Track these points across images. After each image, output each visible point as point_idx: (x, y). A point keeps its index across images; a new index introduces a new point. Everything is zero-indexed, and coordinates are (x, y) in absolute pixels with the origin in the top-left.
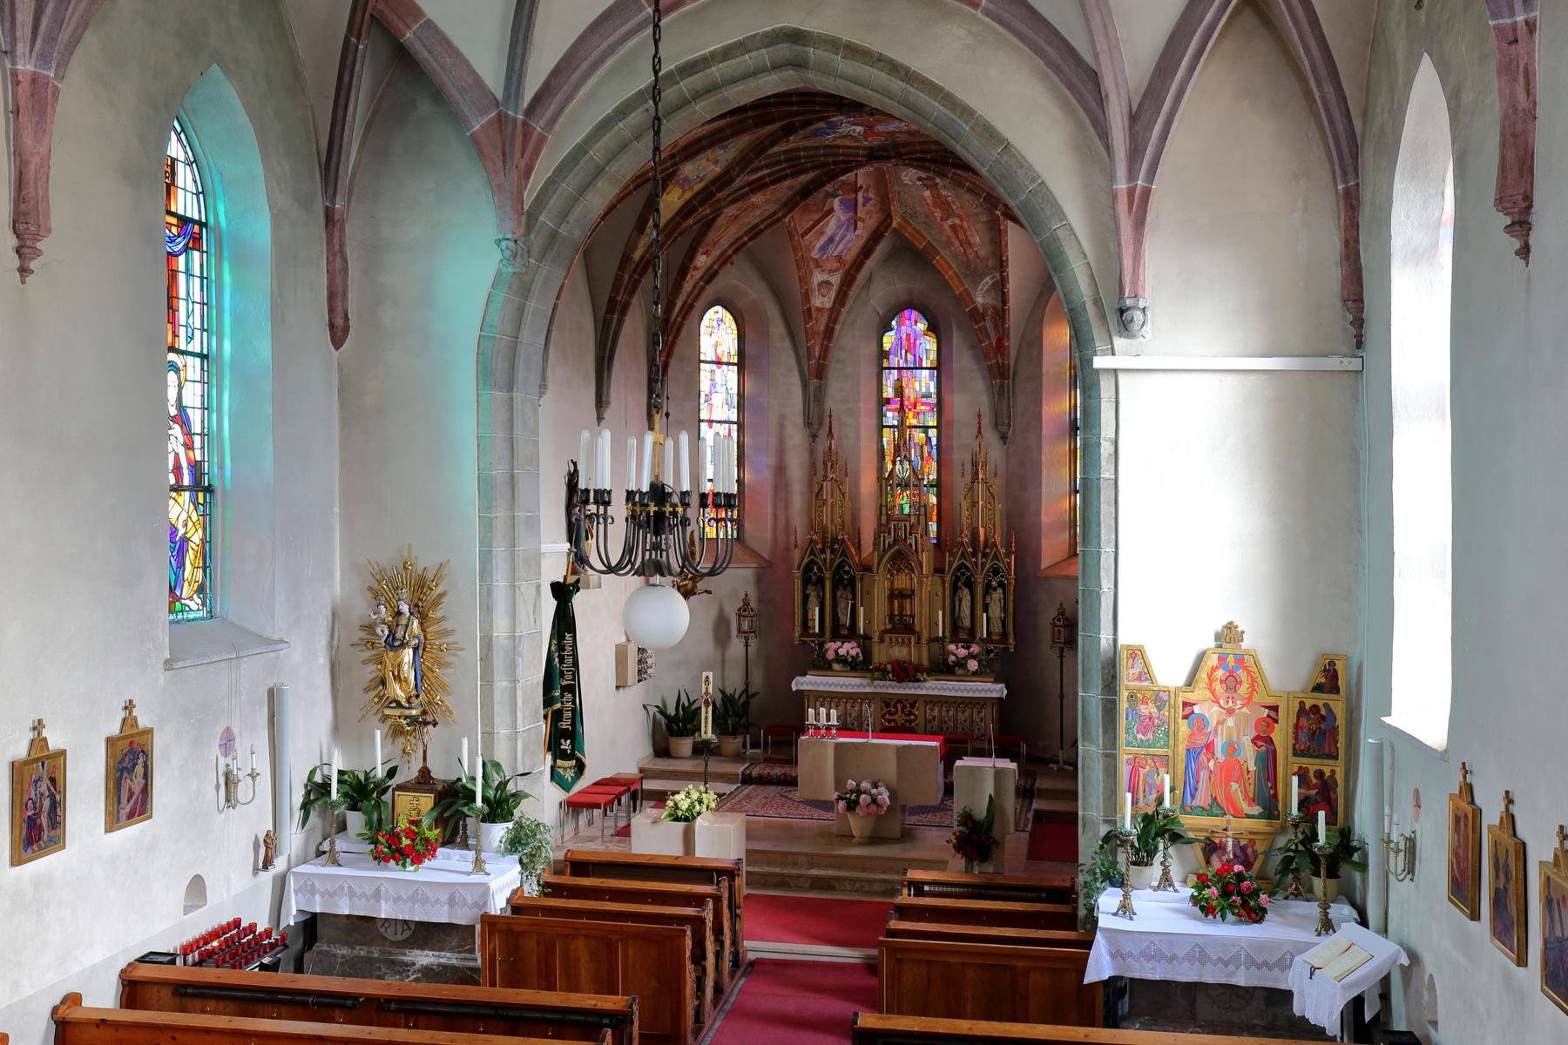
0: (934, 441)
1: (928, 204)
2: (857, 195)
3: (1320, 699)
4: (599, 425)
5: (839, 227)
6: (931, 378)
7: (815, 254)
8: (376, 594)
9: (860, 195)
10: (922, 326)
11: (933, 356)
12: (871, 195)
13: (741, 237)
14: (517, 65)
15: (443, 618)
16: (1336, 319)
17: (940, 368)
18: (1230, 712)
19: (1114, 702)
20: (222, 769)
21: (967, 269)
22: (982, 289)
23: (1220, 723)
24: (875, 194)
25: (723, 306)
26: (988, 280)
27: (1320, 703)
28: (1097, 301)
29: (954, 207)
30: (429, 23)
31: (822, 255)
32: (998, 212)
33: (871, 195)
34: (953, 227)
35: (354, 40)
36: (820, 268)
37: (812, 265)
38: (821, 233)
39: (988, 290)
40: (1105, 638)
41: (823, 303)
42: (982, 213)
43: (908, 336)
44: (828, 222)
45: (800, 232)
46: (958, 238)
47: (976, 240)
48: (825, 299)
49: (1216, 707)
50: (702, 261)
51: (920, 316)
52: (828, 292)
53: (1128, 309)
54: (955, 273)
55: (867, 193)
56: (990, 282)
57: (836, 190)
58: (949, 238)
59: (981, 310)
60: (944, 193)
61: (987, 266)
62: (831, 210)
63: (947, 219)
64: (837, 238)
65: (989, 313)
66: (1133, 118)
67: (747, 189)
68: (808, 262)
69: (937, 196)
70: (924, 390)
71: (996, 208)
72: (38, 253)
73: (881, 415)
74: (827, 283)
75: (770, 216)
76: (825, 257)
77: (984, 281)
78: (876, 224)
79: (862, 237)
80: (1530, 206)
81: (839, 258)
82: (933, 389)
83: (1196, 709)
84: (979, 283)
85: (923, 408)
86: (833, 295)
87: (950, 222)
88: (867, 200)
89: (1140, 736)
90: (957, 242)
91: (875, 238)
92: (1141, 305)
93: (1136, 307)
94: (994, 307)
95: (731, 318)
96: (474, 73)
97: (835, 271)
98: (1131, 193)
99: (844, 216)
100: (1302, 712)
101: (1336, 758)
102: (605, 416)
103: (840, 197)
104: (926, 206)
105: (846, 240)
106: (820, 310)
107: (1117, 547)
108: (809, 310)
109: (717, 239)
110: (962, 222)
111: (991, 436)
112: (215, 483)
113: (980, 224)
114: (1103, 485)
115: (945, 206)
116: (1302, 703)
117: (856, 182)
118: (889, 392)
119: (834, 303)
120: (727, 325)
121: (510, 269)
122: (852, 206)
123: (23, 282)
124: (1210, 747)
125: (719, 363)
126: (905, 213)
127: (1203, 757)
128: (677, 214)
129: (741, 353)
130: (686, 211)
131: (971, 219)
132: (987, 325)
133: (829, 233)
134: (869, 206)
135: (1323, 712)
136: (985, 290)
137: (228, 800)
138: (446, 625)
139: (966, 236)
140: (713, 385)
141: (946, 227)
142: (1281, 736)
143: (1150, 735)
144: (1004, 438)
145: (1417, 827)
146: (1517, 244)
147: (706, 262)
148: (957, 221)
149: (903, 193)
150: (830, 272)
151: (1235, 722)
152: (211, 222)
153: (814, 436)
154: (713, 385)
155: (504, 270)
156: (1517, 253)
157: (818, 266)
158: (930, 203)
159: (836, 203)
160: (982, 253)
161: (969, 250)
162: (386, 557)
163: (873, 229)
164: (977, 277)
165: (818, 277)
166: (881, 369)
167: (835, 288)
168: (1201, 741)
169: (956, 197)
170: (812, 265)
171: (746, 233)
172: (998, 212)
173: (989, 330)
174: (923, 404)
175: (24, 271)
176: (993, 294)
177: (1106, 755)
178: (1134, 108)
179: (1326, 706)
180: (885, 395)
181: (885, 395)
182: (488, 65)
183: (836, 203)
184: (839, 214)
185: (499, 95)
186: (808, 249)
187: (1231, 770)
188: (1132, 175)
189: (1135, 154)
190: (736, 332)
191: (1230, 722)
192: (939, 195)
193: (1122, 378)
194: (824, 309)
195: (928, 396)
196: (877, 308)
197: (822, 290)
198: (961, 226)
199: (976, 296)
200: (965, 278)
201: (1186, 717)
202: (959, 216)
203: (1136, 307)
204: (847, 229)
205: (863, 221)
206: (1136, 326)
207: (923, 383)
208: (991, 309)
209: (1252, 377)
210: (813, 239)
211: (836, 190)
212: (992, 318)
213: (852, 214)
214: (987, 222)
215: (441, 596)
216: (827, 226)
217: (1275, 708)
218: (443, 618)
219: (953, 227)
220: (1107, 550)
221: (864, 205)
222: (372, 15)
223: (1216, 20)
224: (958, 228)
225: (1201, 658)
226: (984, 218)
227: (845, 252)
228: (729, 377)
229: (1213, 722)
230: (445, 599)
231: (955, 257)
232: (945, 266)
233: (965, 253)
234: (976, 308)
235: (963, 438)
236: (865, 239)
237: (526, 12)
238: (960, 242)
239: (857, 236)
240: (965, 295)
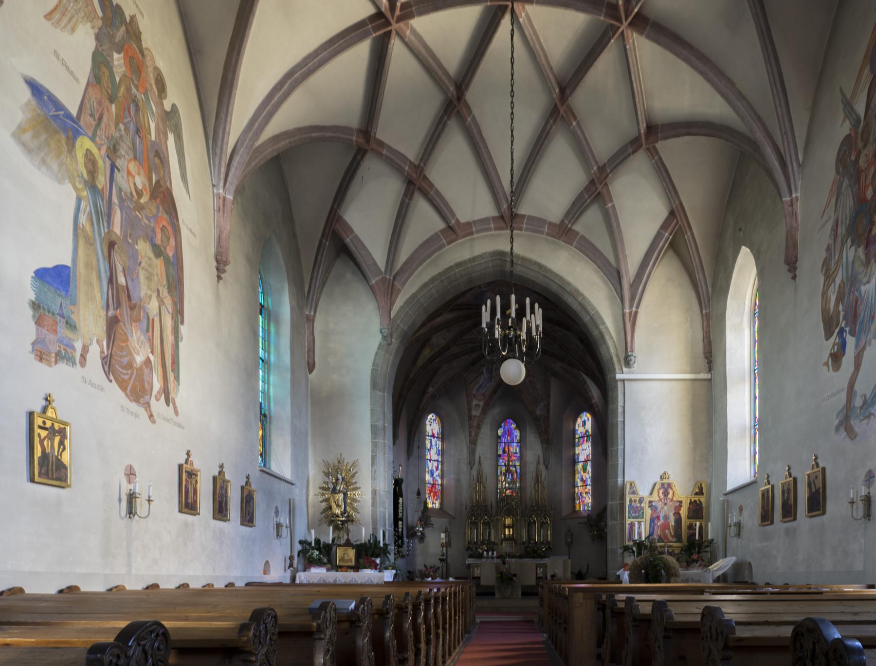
0: (518, 471)
3: (697, 498)
6: (517, 446)
7: (474, 392)
8: (327, 474)
9: (494, 366)
10: (514, 426)
11: (518, 438)
14: (391, 256)
15: (356, 483)
16: (702, 361)
17: (522, 442)
18: (666, 504)
19: (623, 504)
20: (275, 523)
23: (662, 508)
26: (542, 404)
27: (697, 499)
28: (617, 355)
30: (356, 236)
35: (324, 241)
40: (620, 480)
43: (508, 430)
49: (661, 503)
50: (431, 390)
51: (513, 422)
53: (629, 356)
62: (482, 373)
64: (484, 385)
66: (631, 286)
70: (514, 451)
72: (225, 271)
73: (498, 461)
80: (797, 261)
82: (518, 451)
83: (653, 504)
85: (514, 458)
86: (480, 410)
89: (633, 514)
92: (634, 354)
93: (632, 355)
96: (373, 259)
98: (630, 313)
100: (691, 503)
101: (702, 518)
106: (475, 417)
107: (624, 446)
108: (471, 416)
111: (542, 467)
112: (267, 413)
114: (619, 423)
116: (691, 500)
118: (500, 452)
121: (385, 342)
123: (218, 282)
124: (658, 518)
125: (433, 436)
127: (656, 521)
129: (442, 433)
130: (431, 360)
133: (481, 382)
135: (698, 502)
137: (277, 535)
138: (357, 485)
140: (431, 445)
142: (684, 512)
143: (637, 514)
144: (547, 468)
145: (741, 518)
146: (791, 275)
150: (480, 400)
151: (668, 508)
152: (266, 306)
153: (471, 468)
154: (431, 445)
155: (383, 343)
156: (792, 278)
157: (475, 397)
159: (484, 369)
162: (332, 459)
165: (475, 402)
166: (498, 443)
168: (655, 515)
174: (514, 456)
175: (219, 278)
177: (621, 523)
178: (631, 282)
179: (699, 500)
180: (499, 453)
181: (499, 453)
182: (379, 255)
185: (383, 270)
187: (665, 526)
188: (631, 307)
189: (632, 299)
191: (666, 508)
193: (626, 382)
195: (516, 453)
201: (649, 507)
203: (632, 355)
206: (632, 363)
207: (515, 448)
209: (673, 383)
215: (355, 474)
217: (681, 502)
218: (356, 483)
220: (620, 447)
222: (333, 230)
223: (664, 245)
225: (655, 485)
228: (437, 444)
229: (659, 509)
230: (357, 475)
235: (531, 469)
237: (398, 230)
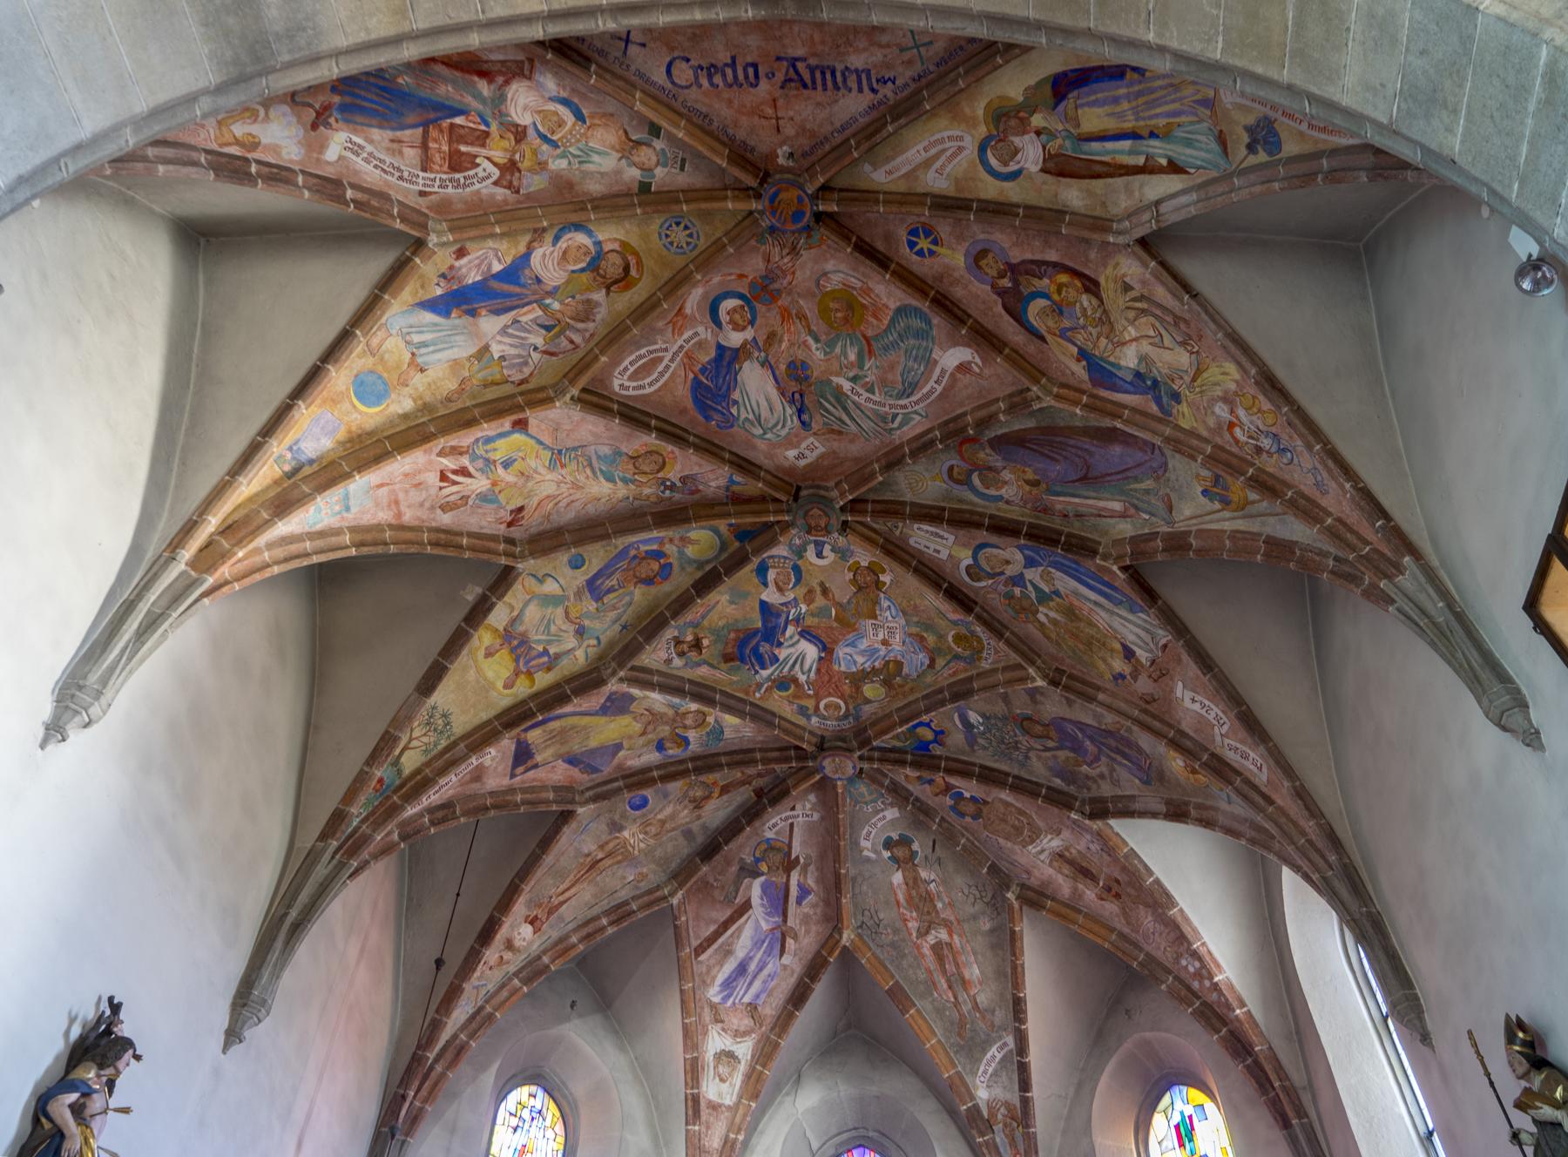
1: (898, 903)
2: (789, 876)
4: (224, 1052)
5: (757, 944)
7: (714, 994)
9: (795, 877)
12: (811, 882)
13: (596, 918)
21: (959, 1035)
22: (985, 1072)
24: (817, 882)
25: (546, 1090)
29: (939, 905)
31: (725, 999)
32: (1009, 895)
33: (811, 882)
34: (937, 948)
36: (720, 1025)
37: (707, 1015)
38: (727, 952)
39: (995, 1074)
41: (720, 1095)
42: (984, 913)
44: (740, 930)
45: (695, 943)
46: (944, 972)
47: (973, 972)
48: (725, 1087)
52: (731, 1075)
54: (939, 1041)
55: (805, 877)
56: (999, 1056)
57: (757, 860)
58: (929, 971)
59: (985, 1114)
60: (924, 874)
61: (993, 1025)
62: (746, 906)
63: (927, 932)
64: (752, 967)
65: (1000, 1117)
67: (621, 783)
68: (702, 1008)
69: (913, 882)
71: (1008, 889)
74: (730, 1055)
75: (650, 892)
76: (730, 1002)
77: (989, 1056)
78: (814, 948)
79: (793, 972)
81: (752, 1008)
84: (980, 1060)
86: (738, 1079)
87: (931, 939)
88: (804, 892)
90: (943, 981)
91: (813, 970)
94: (1007, 1104)
95: (558, 1114)
97: (745, 1034)
99: (767, 921)
102: (247, 1034)
103: (762, 879)
104: (896, 908)
105: (765, 972)
106: (714, 1107)
109: (555, 901)
110: (951, 936)
113: (979, 938)
115: (921, 900)
117: (790, 846)
119: (740, 1097)
120: (548, 1122)
122: (779, 902)
126: (861, 927)
128: (497, 717)
131: (966, 926)
132: (998, 1140)
133: (740, 953)
134: (806, 908)
136: (990, 1070)
139: (957, 965)
141: (927, 951)
147: (531, 943)
148: (943, 935)
149: (859, 880)
150: (738, 1034)
157: (718, 1020)
158: (901, 897)
159: (756, 889)
160: (983, 999)
161: (962, 996)
163: (810, 957)
164: (973, 1048)
165: (716, 1041)
167: (742, 1068)
169: (944, 882)
170: (707, 1015)
171: (607, 913)
172: (1009, 895)
173: (1002, 1150)
176: (1004, 1078)
183: (756, 889)
184: (758, 920)
186: (704, 982)
190: (561, 1140)
192: (916, 879)
194: (720, 1105)
196: (809, 1134)
197: (721, 1069)
198: (949, 945)
199: (976, 1088)
200: (956, 1053)
202: (947, 924)
204: (768, 953)
205: (795, 938)
208: (1003, 1110)
210: (712, 961)
211: (757, 860)
212: (1005, 1125)
213: (778, 919)
214: (992, 931)
216: (738, 937)
219: (937, 948)
221: (799, 902)
224: (946, 952)
226: (986, 925)
227: (763, 996)
231: (939, 1011)
232: (926, 1032)
233: (957, 1004)
234: (976, 1108)
236: (795, 976)
238: (948, 981)
239: (785, 967)
240: (957, 1081)
